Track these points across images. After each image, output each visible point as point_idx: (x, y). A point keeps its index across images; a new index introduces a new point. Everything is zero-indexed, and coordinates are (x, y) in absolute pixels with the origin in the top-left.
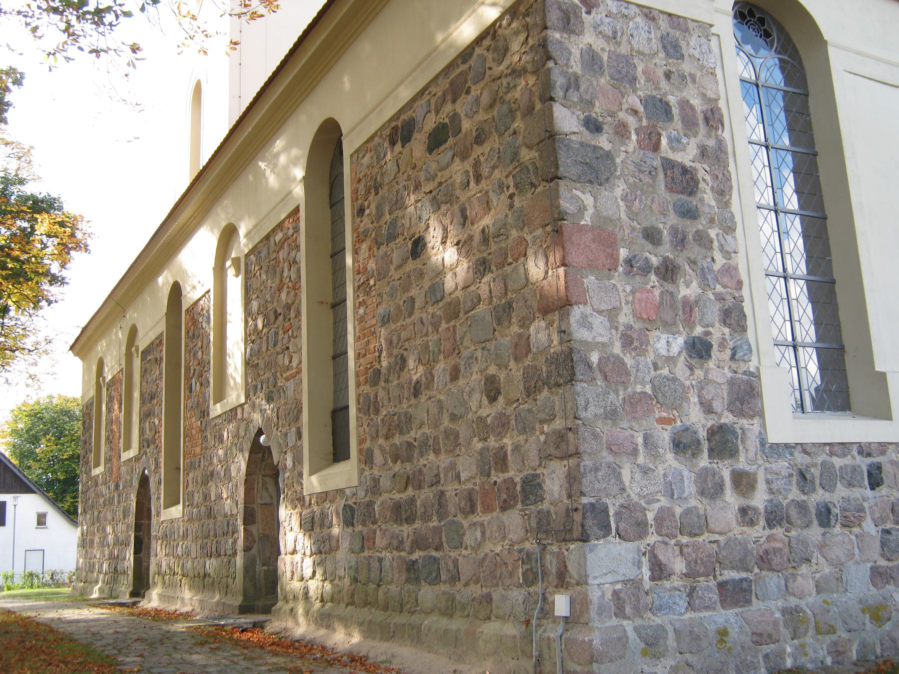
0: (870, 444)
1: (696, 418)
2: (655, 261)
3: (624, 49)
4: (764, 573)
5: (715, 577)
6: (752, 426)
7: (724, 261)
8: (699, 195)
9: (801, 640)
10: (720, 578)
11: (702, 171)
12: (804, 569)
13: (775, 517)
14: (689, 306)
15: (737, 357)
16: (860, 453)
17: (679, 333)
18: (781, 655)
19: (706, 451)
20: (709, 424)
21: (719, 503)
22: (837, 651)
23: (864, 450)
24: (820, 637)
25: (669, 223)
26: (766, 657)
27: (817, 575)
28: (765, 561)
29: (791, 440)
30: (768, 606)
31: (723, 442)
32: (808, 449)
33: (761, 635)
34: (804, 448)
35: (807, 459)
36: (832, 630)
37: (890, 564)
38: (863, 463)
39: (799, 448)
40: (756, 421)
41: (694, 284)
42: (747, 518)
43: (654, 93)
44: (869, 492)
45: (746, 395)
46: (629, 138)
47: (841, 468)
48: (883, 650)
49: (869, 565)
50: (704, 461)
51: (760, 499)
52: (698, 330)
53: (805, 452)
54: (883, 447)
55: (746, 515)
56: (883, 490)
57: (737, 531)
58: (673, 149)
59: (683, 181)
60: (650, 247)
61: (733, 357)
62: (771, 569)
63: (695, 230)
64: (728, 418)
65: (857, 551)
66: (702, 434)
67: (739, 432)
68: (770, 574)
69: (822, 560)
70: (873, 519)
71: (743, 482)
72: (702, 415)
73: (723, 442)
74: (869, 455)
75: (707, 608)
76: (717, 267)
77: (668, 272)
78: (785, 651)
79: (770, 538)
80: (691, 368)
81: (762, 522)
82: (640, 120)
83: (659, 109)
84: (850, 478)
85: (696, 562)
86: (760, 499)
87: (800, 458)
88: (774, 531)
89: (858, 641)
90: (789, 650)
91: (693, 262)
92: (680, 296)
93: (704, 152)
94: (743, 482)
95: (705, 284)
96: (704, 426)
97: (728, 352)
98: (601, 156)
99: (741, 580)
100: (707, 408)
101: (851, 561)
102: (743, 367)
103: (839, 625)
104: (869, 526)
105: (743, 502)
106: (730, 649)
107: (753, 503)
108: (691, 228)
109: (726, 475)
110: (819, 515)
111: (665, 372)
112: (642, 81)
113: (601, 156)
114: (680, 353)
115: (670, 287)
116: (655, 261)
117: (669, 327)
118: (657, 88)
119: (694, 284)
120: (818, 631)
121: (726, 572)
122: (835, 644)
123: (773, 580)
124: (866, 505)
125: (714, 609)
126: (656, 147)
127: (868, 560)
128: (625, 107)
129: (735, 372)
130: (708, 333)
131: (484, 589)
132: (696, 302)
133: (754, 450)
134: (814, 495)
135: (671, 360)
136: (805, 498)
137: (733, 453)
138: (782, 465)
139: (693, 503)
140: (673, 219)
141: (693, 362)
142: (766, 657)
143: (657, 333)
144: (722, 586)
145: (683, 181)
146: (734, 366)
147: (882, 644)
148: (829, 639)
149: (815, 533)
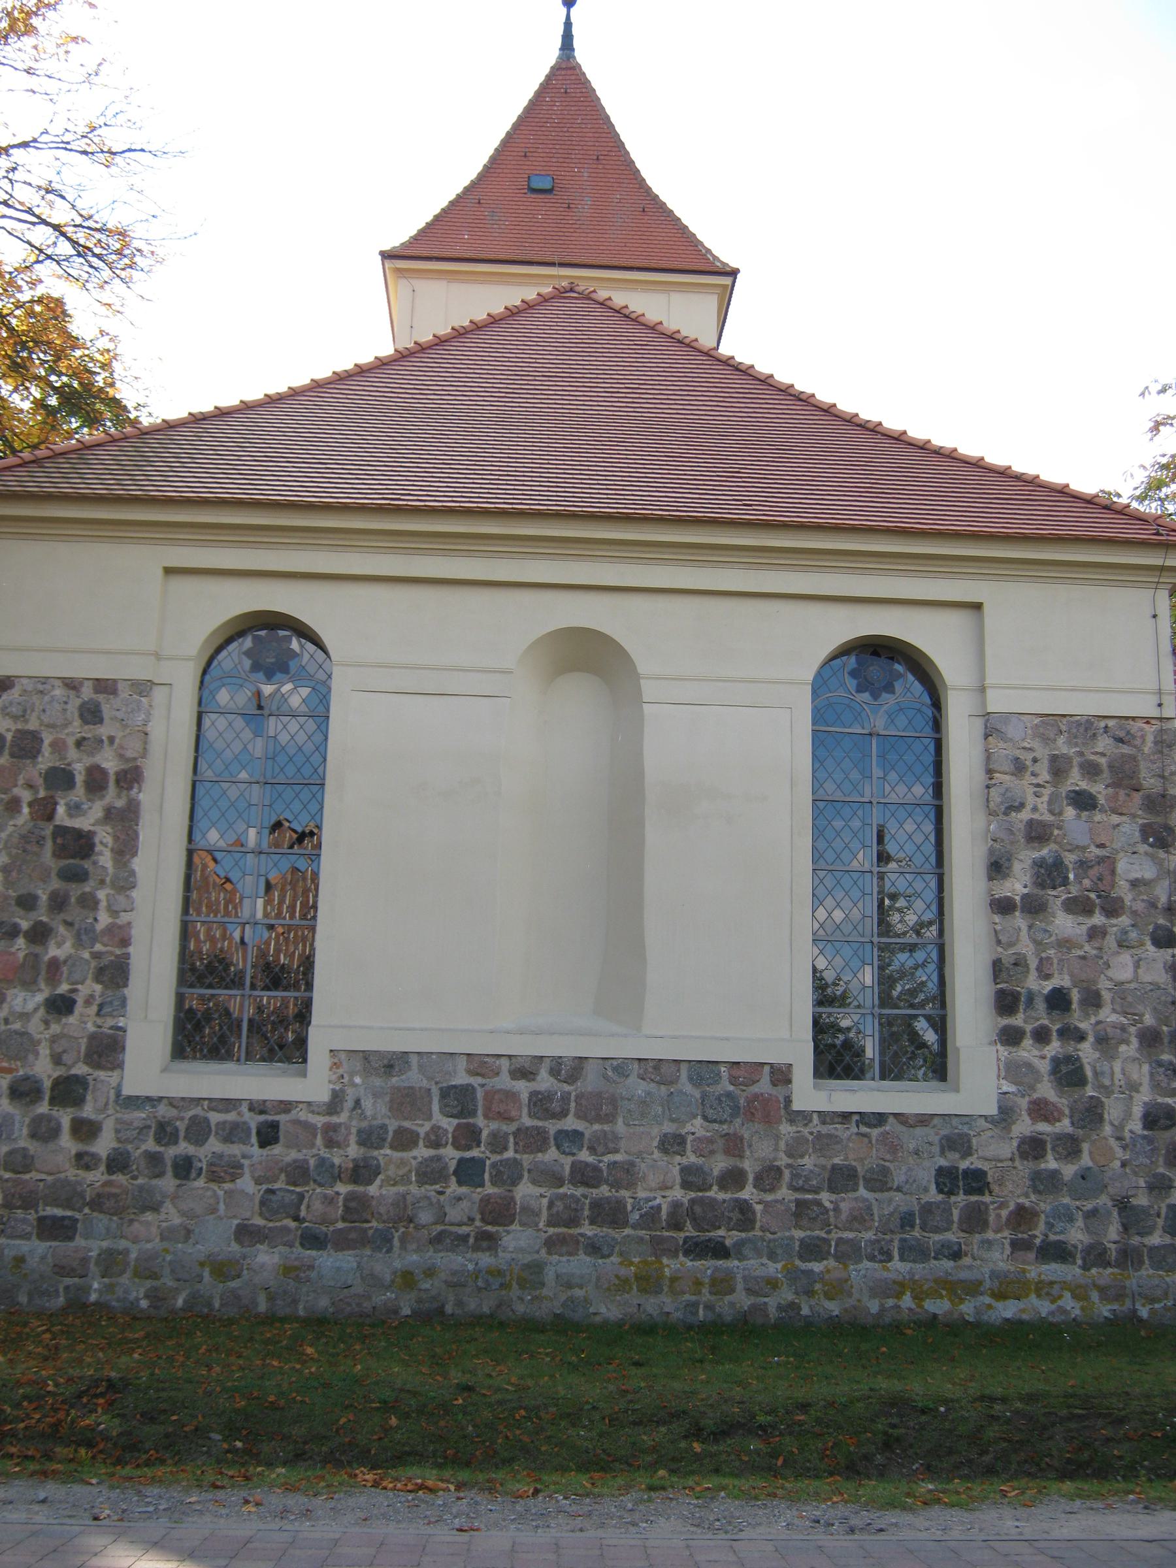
0: (265, 1101)
1: (43, 1069)
2: (25, 925)
3: (33, 725)
4: (95, 1214)
5: (37, 1212)
6: (112, 1078)
7: (110, 920)
8: (94, 858)
9: (114, 1280)
10: (42, 1213)
11: (104, 837)
12: (149, 1216)
13: (117, 1163)
14: (55, 965)
15: (102, 1012)
16: (251, 1109)
17: (39, 990)
18: (87, 1290)
19: (47, 1098)
20: (55, 1075)
21: (51, 1146)
22: (155, 1296)
23: (258, 1107)
24: (137, 1280)
25: (50, 889)
26: (67, 1288)
27: (164, 1224)
28: (97, 1204)
29: (153, 1092)
30: (89, 1245)
31: (69, 1091)
32: (175, 1103)
33: (63, 1267)
34: (171, 1102)
35: (173, 1112)
36: (154, 1276)
37: (271, 1225)
38: (253, 1121)
39: (165, 1101)
40: (116, 1073)
41: (68, 944)
42: (82, 1162)
43: (57, 764)
44: (255, 1150)
45: (107, 1050)
46: (19, 812)
47: (218, 1124)
48: (222, 1305)
49: (236, 1222)
50: (43, 1108)
51: (103, 1146)
52: (64, 988)
53: (171, 1104)
54: (286, 1106)
55: (84, 1161)
56: (277, 1150)
57: (72, 1173)
58: (71, 816)
59: (78, 845)
60: (22, 912)
61: (98, 1014)
62: (101, 1212)
63: (79, 892)
64: (81, 1069)
65: (222, 1206)
66: (47, 1084)
67: (92, 1083)
68: (101, 1216)
69: (172, 1210)
70: (253, 1177)
71: (85, 1130)
72: (51, 1066)
73: (69, 1091)
74: (262, 1112)
75: (21, 1237)
76: (100, 927)
77: (39, 935)
78: (91, 1287)
79: (107, 1184)
80: (47, 1023)
81: (103, 1168)
82: (37, 792)
83: (60, 779)
84: (232, 1133)
85: (13, 1196)
86: (103, 1146)
87: (163, 1111)
88: (114, 1177)
89: (188, 1291)
90: (96, 1285)
91: (68, 924)
92: (46, 958)
93: (109, 815)
94: (85, 1130)
95: (79, 943)
96: (49, 1077)
97: (95, 1008)
98: (1167, 496)
99: (63, 1218)
100: (57, 1060)
101: (212, 1216)
102: (110, 1022)
103: (167, 1271)
104: (246, 1184)
105: (81, 1147)
106: (26, 1274)
107: (93, 1149)
108: (75, 891)
109: (66, 1123)
110: (176, 1166)
111: (17, 1026)
112: (47, 754)
113: (1167, 496)
114: (36, 1010)
115: (38, 949)
116: (25, 925)
117: (29, 985)
118: (63, 758)
119: (68, 944)
120: (137, 1274)
121: (48, 1208)
122: (156, 1289)
123: (101, 1221)
124: (246, 1162)
125: (29, 1239)
126: (50, 817)
127: (235, 1217)
128: (21, 782)
129: (100, 1027)
130: (75, 991)
131: (630, 1201)
132: (65, 962)
133: (104, 1100)
134: (174, 1147)
135: (25, 1016)
136: (162, 1149)
137: (79, 1102)
138: (139, 1116)
139: (22, 1144)
140: (56, 884)
141: (49, 1018)
142: (67, 1288)
143: (16, 991)
144: (41, 1220)
145: (78, 845)
146: (99, 1021)
147: (222, 1299)
148: (149, 1283)
149: (168, 1183)
